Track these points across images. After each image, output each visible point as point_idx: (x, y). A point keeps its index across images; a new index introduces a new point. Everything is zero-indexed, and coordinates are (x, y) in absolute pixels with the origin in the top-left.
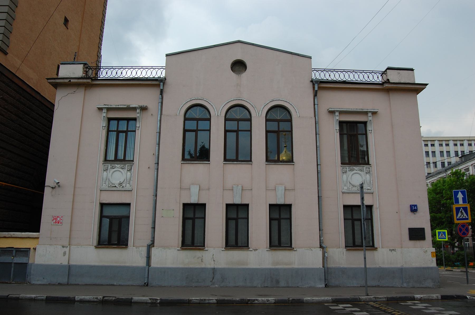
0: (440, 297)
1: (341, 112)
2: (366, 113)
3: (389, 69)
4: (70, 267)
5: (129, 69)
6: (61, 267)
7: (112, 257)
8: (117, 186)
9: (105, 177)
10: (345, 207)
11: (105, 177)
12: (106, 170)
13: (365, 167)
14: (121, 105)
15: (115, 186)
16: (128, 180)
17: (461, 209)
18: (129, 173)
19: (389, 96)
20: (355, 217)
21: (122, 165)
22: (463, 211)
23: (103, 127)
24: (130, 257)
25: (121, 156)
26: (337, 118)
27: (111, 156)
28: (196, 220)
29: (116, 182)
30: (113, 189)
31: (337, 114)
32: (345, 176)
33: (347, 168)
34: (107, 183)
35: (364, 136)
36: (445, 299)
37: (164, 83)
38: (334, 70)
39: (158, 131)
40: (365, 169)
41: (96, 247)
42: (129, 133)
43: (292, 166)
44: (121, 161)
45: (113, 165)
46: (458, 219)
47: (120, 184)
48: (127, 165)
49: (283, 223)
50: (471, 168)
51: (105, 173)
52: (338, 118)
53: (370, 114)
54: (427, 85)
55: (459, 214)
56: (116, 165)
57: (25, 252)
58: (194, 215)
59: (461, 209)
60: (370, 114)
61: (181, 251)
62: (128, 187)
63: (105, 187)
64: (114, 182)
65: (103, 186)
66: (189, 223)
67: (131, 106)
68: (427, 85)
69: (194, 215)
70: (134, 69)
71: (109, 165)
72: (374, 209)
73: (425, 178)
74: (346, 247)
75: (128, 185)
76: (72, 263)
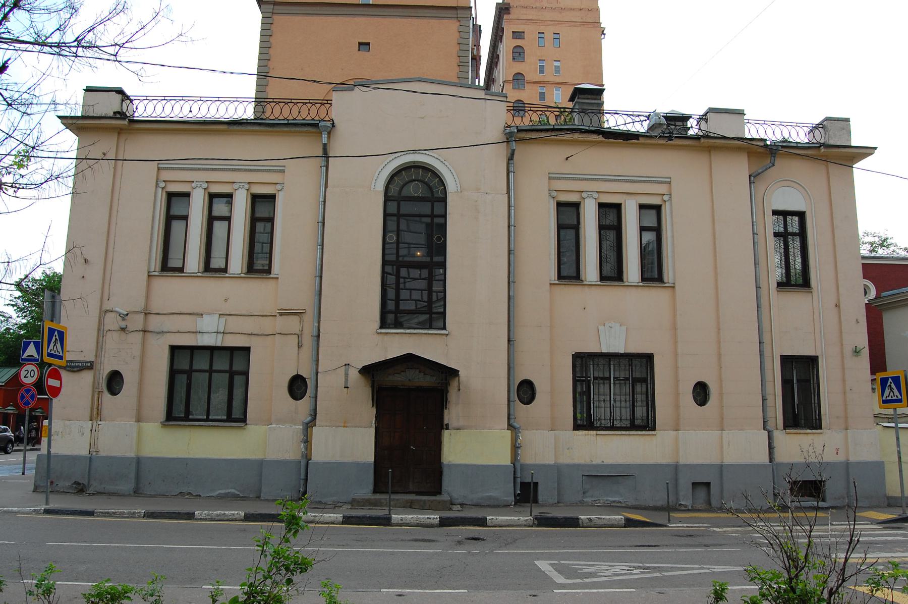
0: (437, 521)
3: (711, 110)
4: (139, 461)
5: (286, 103)
17: (890, 380)
20: (236, 368)
22: (893, 386)
28: (194, 374)
35: (573, 232)
36: (188, 514)
37: (329, 133)
38: (765, 122)
39: (321, 219)
41: (164, 425)
46: (50, 355)
49: (238, 379)
54: (875, 148)
55: (887, 391)
58: (211, 365)
59: (890, 380)
66: (182, 379)
68: (875, 148)
69: (211, 365)
70: (296, 104)
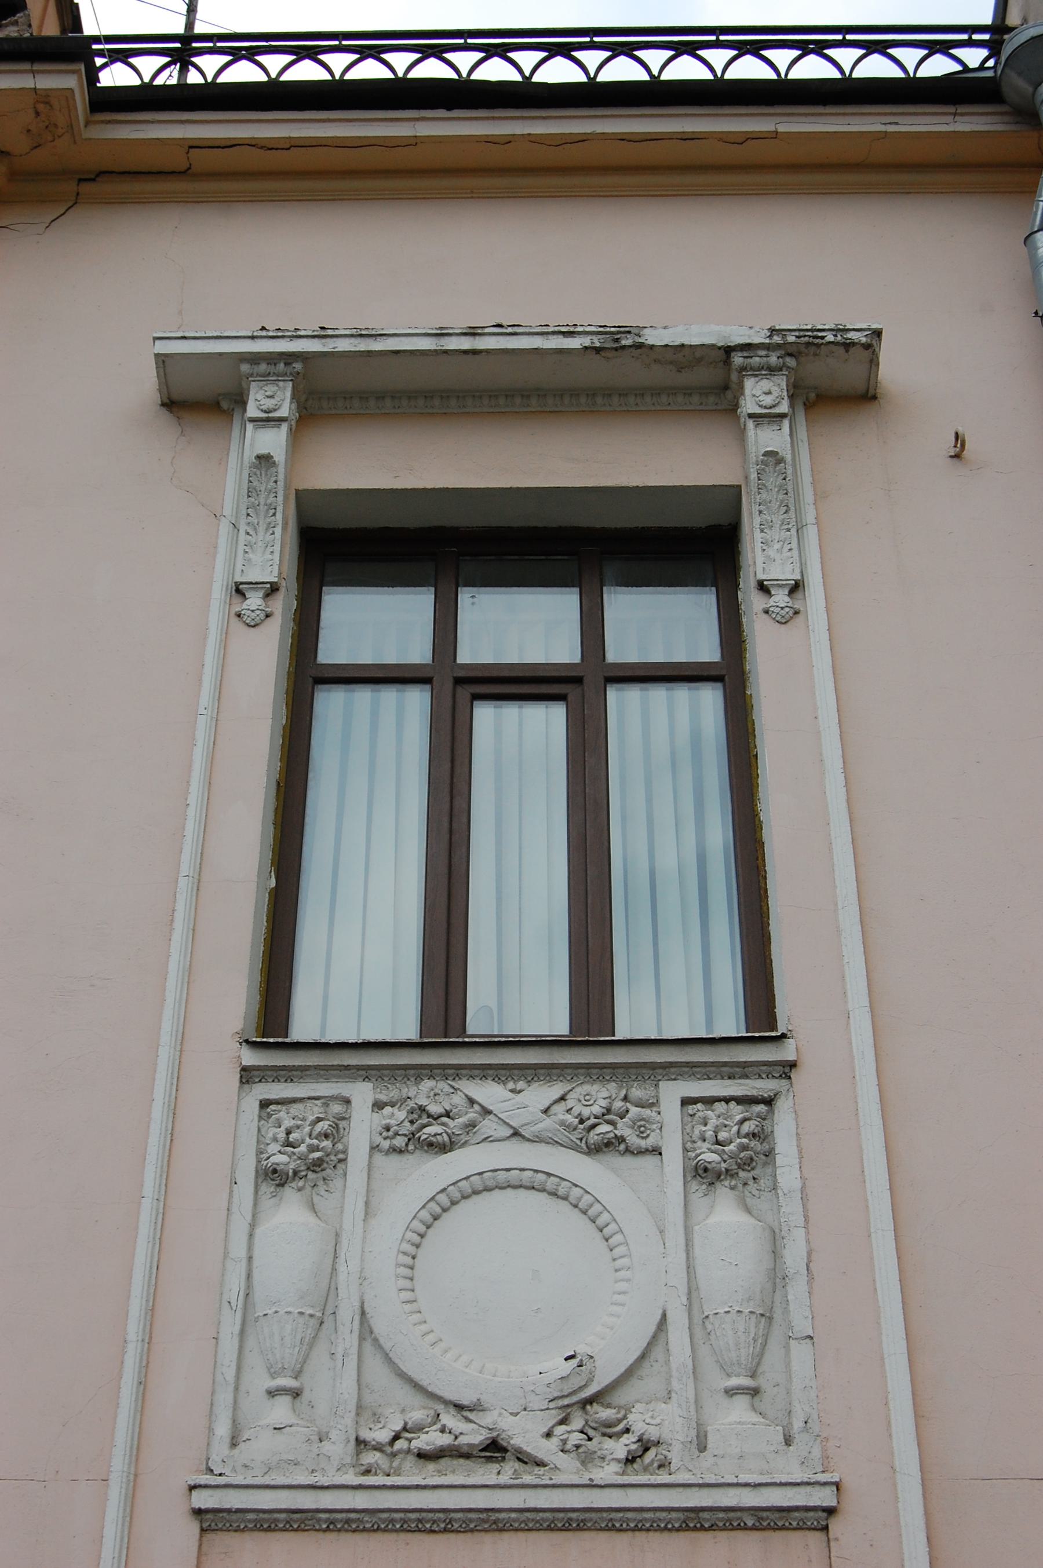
8: (525, 1432)
12: (304, 1169)
15: (494, 1449)
16: (733, 1336)
18: (724, 1215)
23: (239, 591)
25: (520, 984)
27: (360, 975)
29: (511, 1381)
34: (333, 1385)
39: (204, 1558)
42: (623, 705)
44: (518, 1057)
45: (422, 1093)
47: (587, 1405)
48: (672, 1092)
50: (754, 392)
51: (289, 1215)
56: (489, 1093)
62: (741, 1454)
63: (286, 1452)
64: (455, 1373)
65: (261, 1447)
73: (960, 430)
75: (739, 1410)
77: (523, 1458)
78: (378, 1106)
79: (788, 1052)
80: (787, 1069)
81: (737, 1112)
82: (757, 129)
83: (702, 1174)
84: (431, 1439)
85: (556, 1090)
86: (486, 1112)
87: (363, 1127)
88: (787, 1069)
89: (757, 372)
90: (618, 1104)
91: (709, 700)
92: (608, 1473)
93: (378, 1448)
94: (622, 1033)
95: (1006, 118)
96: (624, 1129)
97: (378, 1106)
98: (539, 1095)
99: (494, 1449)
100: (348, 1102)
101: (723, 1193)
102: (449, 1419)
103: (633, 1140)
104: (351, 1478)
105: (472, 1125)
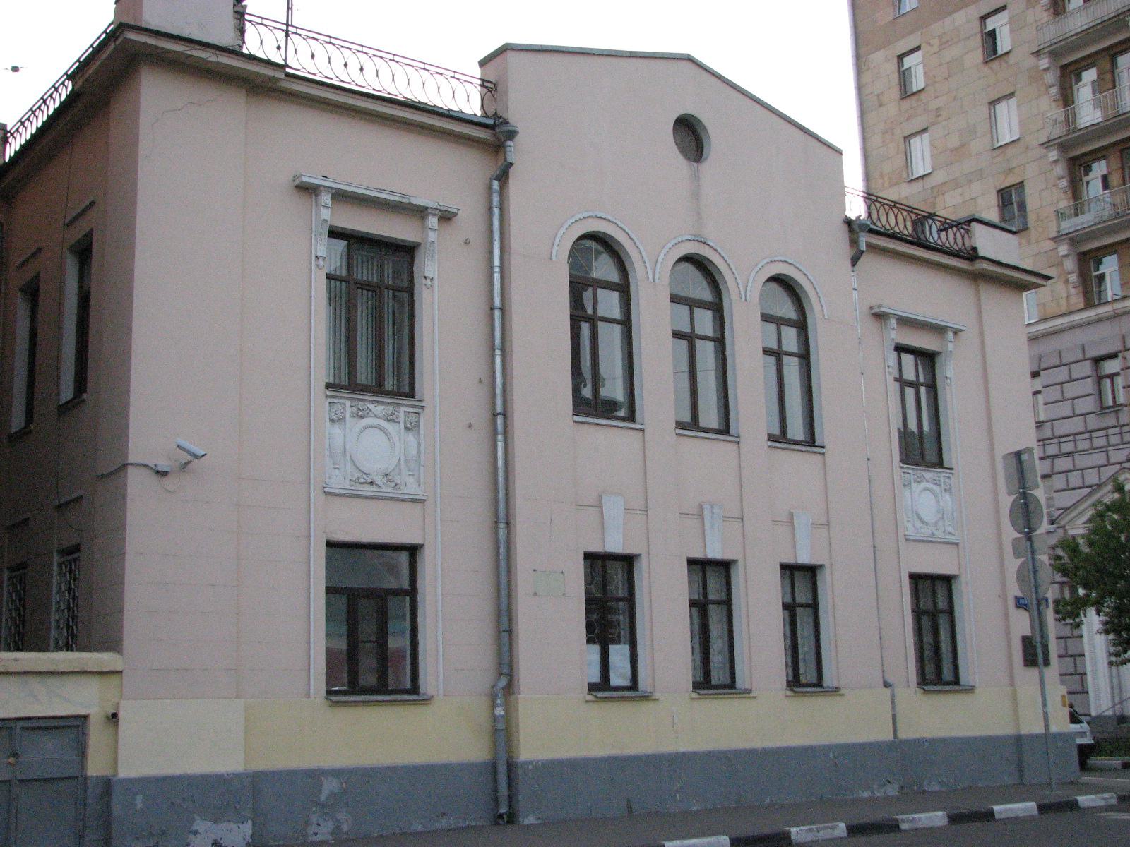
1: (341, 196)
2: (420, 212)
6: (1010, 737)
7: (377, 737)
8: (378, 480)
9: (339, 442)
10: (916, 578)
11: (339, 442)
13: (403, 409)
14: (381, 190)
18: (411, 438)
19: (978, 291)
21: (391, 409)
24: (431, 732)
26: (893, 335)
30: (367, 491)
31: (326, 199)
32: (337, 430)
33: (346, 404)
40: (402, 414)
43: (819, 457)
48: (403, 409)
49: (943, 622)
52: (328, 213)
53: (433, 221)
56: (371, 406)
57: (73, 727)
60: (433, 221)
61: (596, 706)
62: (411, 489)
63: (339, 481)
64: (366, 466)
67: (414, 201)
71: (348, 403)
72: (826, 583)
74: (329, 693)
76: (903, 734)
77: (377, 485)
78: (351, 406)
79: (423, 404)
80: (423, 407)
81: (413, 415)
82: (461, 131)
83: (407, 428)
84: (362, 480)
85: (383, 407)
86: (370, 410)
87: (349, 410)
88: (423, 407)
89: (432, 214)
90: (394, 412)
91: (1068, 379)
92: (389, 490)
93: (353, 481)
94: (816, 444)
95: (490, 135)
96: (394, 417)
97: (351, 406)
98: (381, 408)
99: (372, 483)
100: (345, 404)
101: (336, 426)
102: (365, 476)
103: (396, 420)
104: (349, 487)
105: (368, 413)
